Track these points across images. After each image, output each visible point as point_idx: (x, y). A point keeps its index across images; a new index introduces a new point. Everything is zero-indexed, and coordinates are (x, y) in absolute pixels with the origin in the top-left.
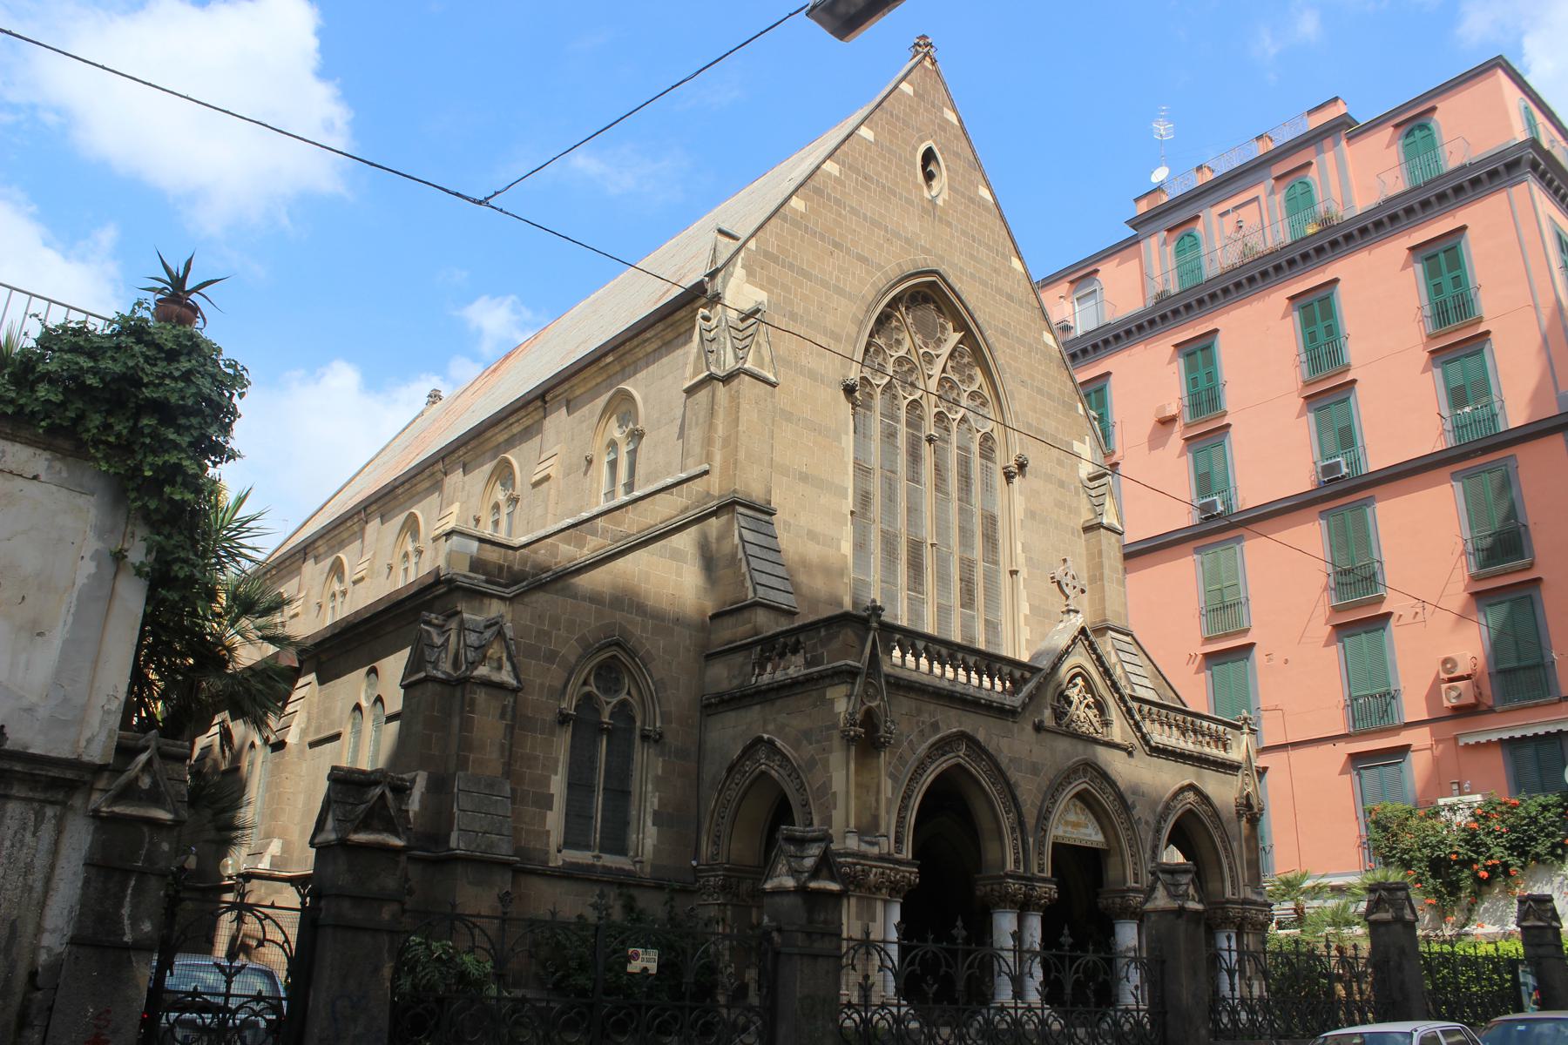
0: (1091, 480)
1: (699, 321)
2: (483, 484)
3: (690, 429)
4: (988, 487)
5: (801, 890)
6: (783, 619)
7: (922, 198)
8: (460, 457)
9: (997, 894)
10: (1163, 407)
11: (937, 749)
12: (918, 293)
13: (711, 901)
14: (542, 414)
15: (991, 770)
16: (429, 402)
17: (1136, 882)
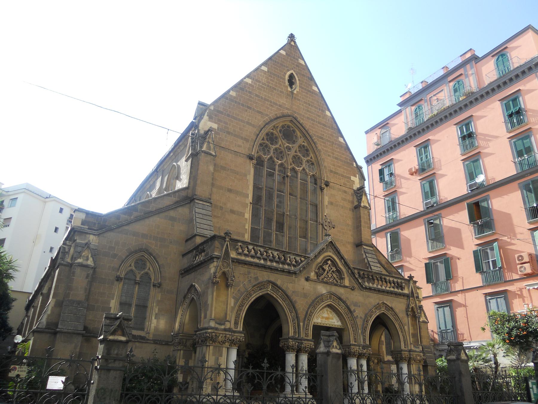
7: (287, 91)
17: (356, 342)
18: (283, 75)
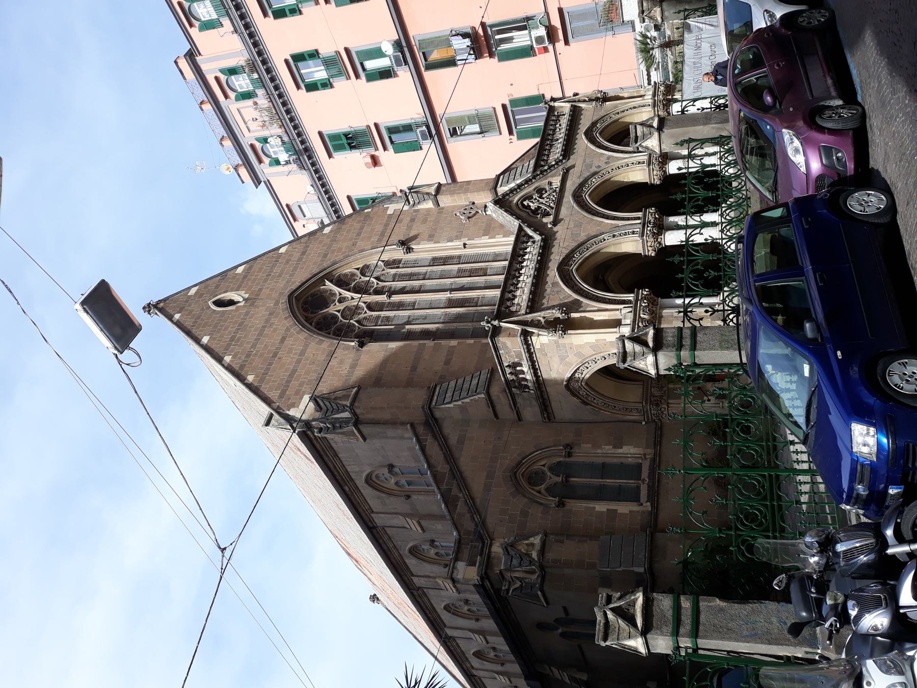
4: (415, 264)
7: (244, 306)
12: (302, 307)
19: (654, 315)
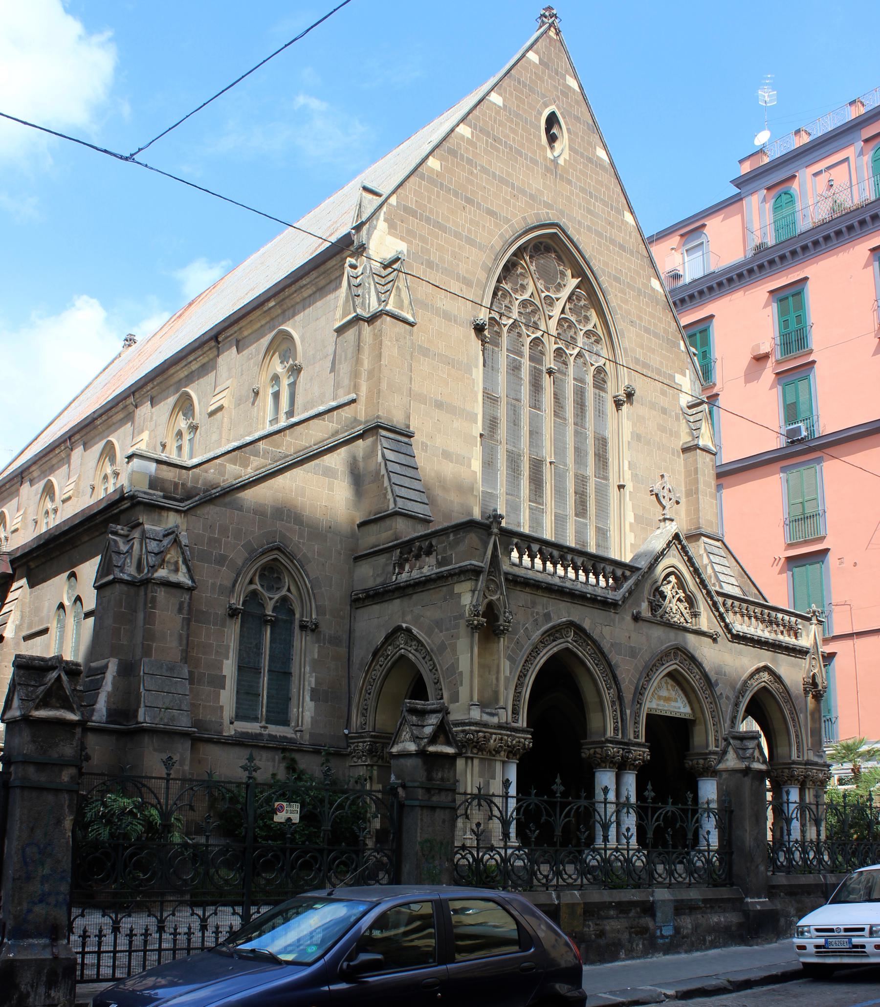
0: (690, 407)
1: (347, 269)
2: (167, 415)
3: (340, 363)
4: (600, 413)
5: (421, 753)
6: (419, 526)
7: (545, 158)
8: (148, 391)
9: (598, 756)
10: (758, 346)
11: (549, 636)
12: (541, 243)
13: (360, 762)
14: (216, 353)
15: (595, 653)
16: (125, 345)
18: (535, 116)
19: (494, 753)
